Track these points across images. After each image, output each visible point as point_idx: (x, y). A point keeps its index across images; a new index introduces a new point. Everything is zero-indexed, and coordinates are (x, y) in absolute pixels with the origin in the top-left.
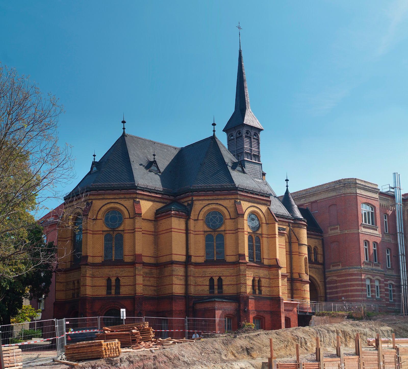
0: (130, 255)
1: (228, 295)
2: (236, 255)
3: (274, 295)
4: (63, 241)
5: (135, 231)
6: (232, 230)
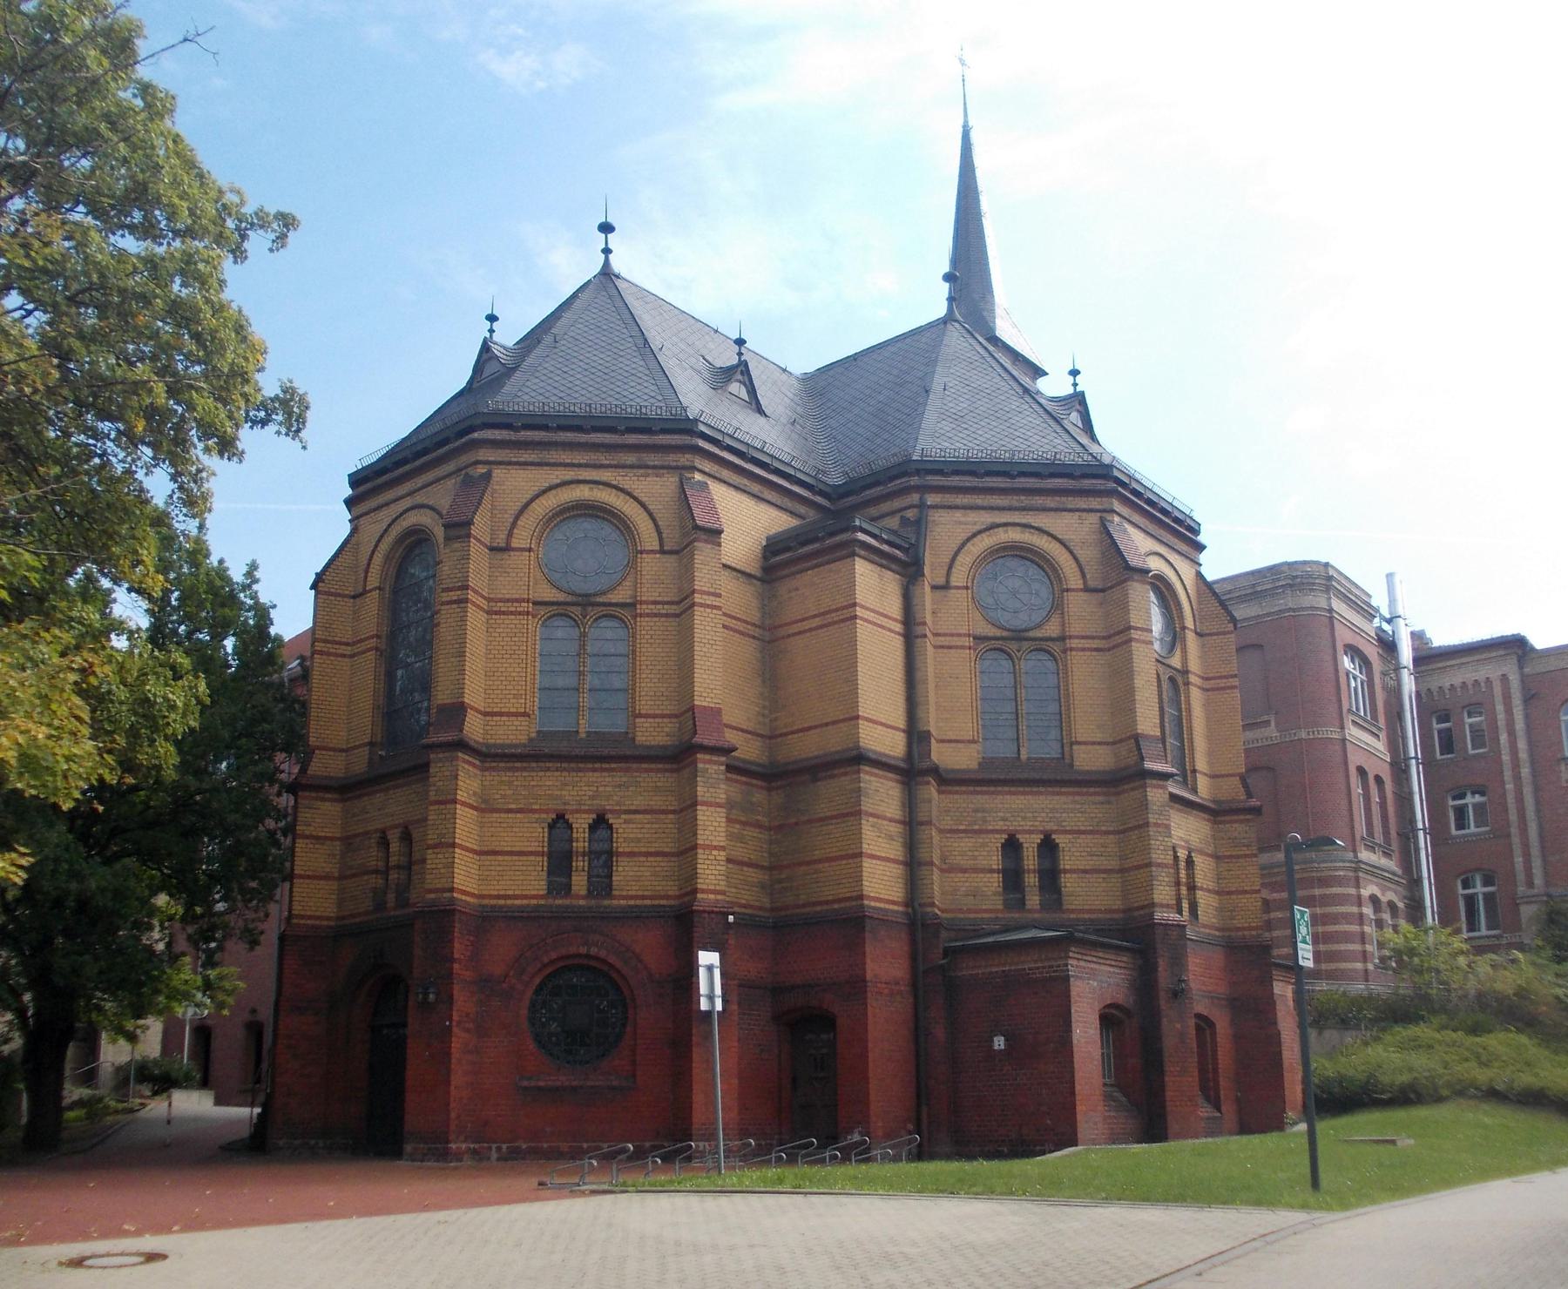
0: (663, 716)
1: (1086, 916)
2: (1114, 743)
3: (1238, 929)
4: (337, 655)
5: (693, 605)
6: (1093, 638)
